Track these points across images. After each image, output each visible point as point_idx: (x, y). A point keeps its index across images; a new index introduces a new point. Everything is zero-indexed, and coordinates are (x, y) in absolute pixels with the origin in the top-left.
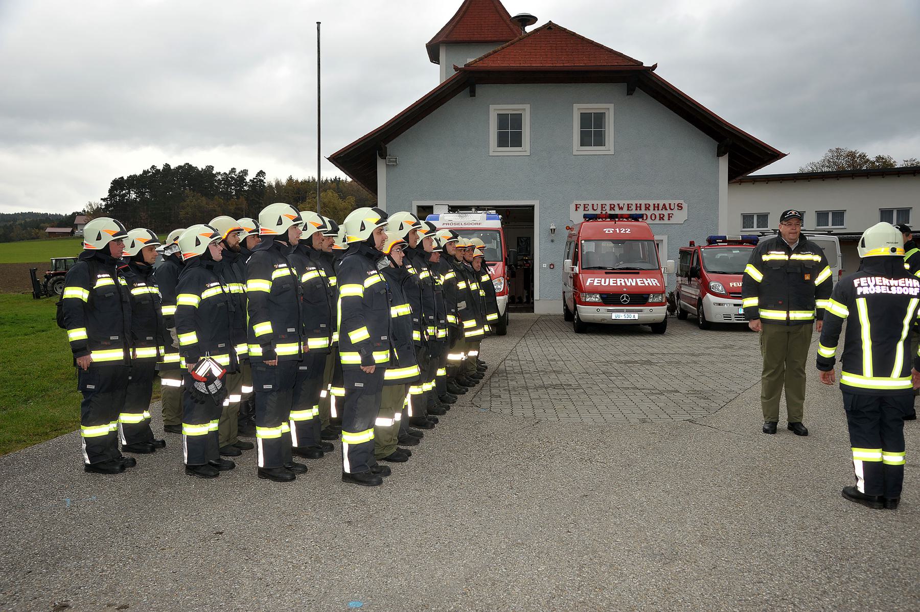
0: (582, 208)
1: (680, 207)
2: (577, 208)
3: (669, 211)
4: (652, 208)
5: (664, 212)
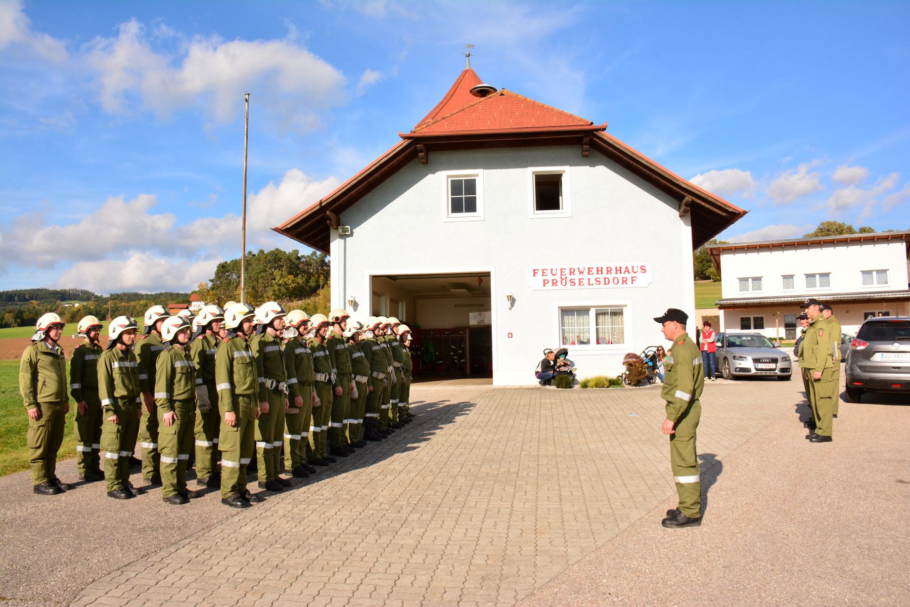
0: (540, 273)
1: (643, 269)
2: (535, 272)
3: (632, 274)
4: (614, 271)
5: (627, 275)
